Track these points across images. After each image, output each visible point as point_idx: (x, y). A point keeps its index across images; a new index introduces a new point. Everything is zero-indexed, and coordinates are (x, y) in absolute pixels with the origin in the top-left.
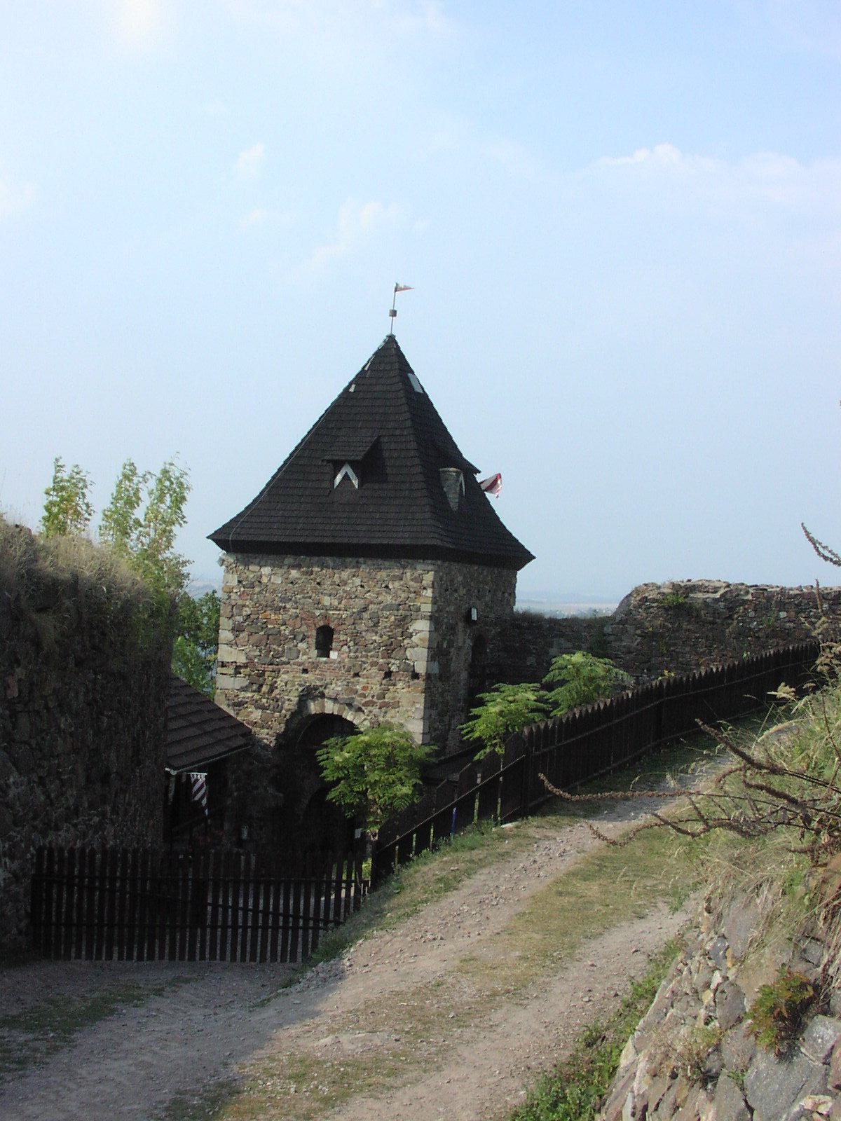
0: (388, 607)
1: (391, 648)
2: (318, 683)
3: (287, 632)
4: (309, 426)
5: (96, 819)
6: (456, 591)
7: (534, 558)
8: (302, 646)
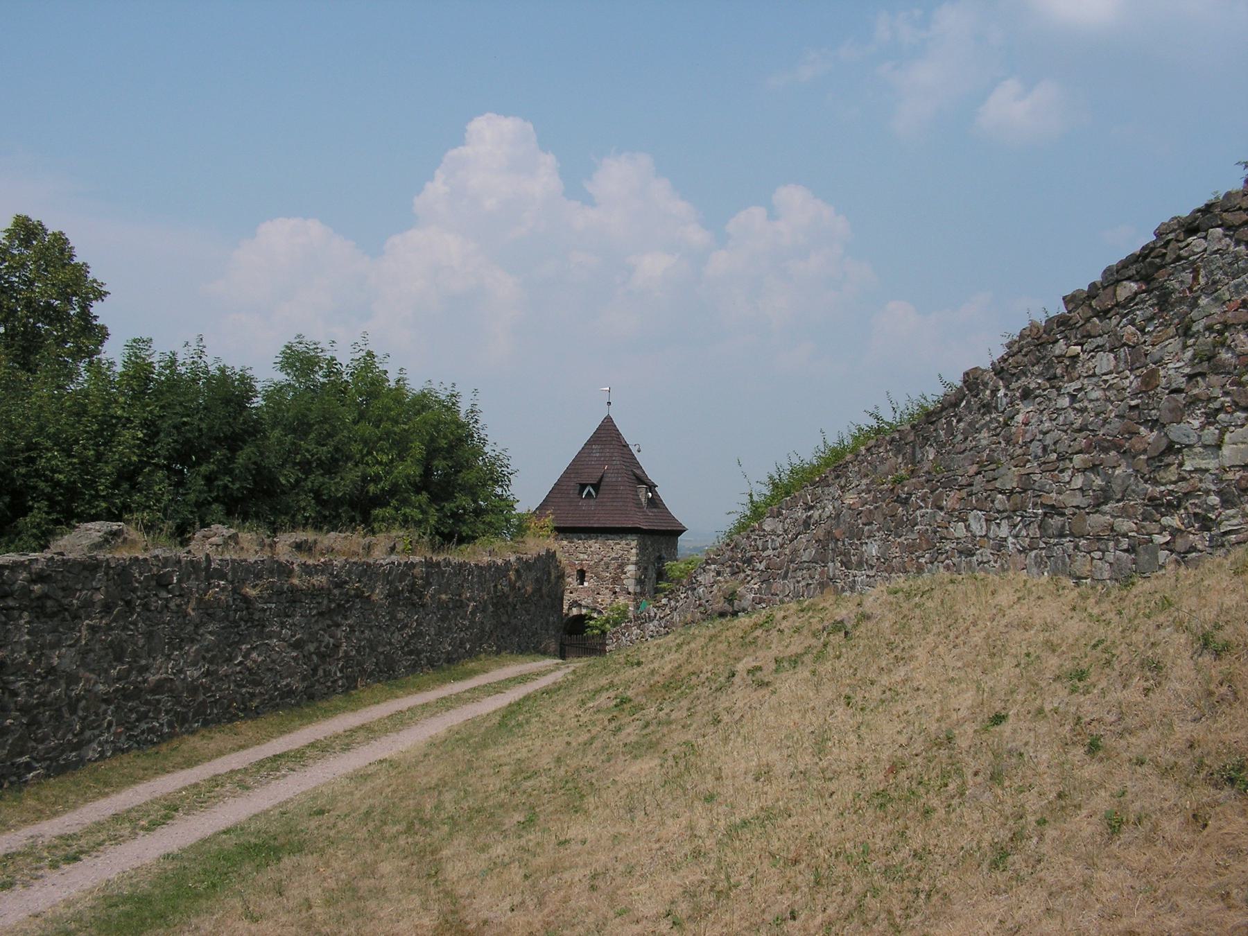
0: (613, 559)
1: (616, 580)
7: (607, 435)
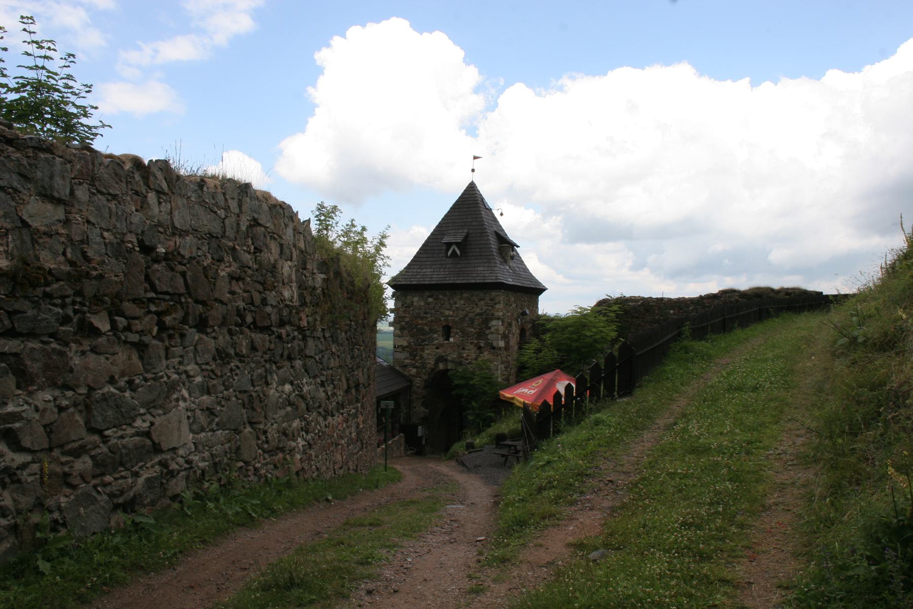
2: (444, 354)
3: (427, 329)
4: (451, 205)
5: (353, 411)
6: (511, 305)
8: (435, 336)
